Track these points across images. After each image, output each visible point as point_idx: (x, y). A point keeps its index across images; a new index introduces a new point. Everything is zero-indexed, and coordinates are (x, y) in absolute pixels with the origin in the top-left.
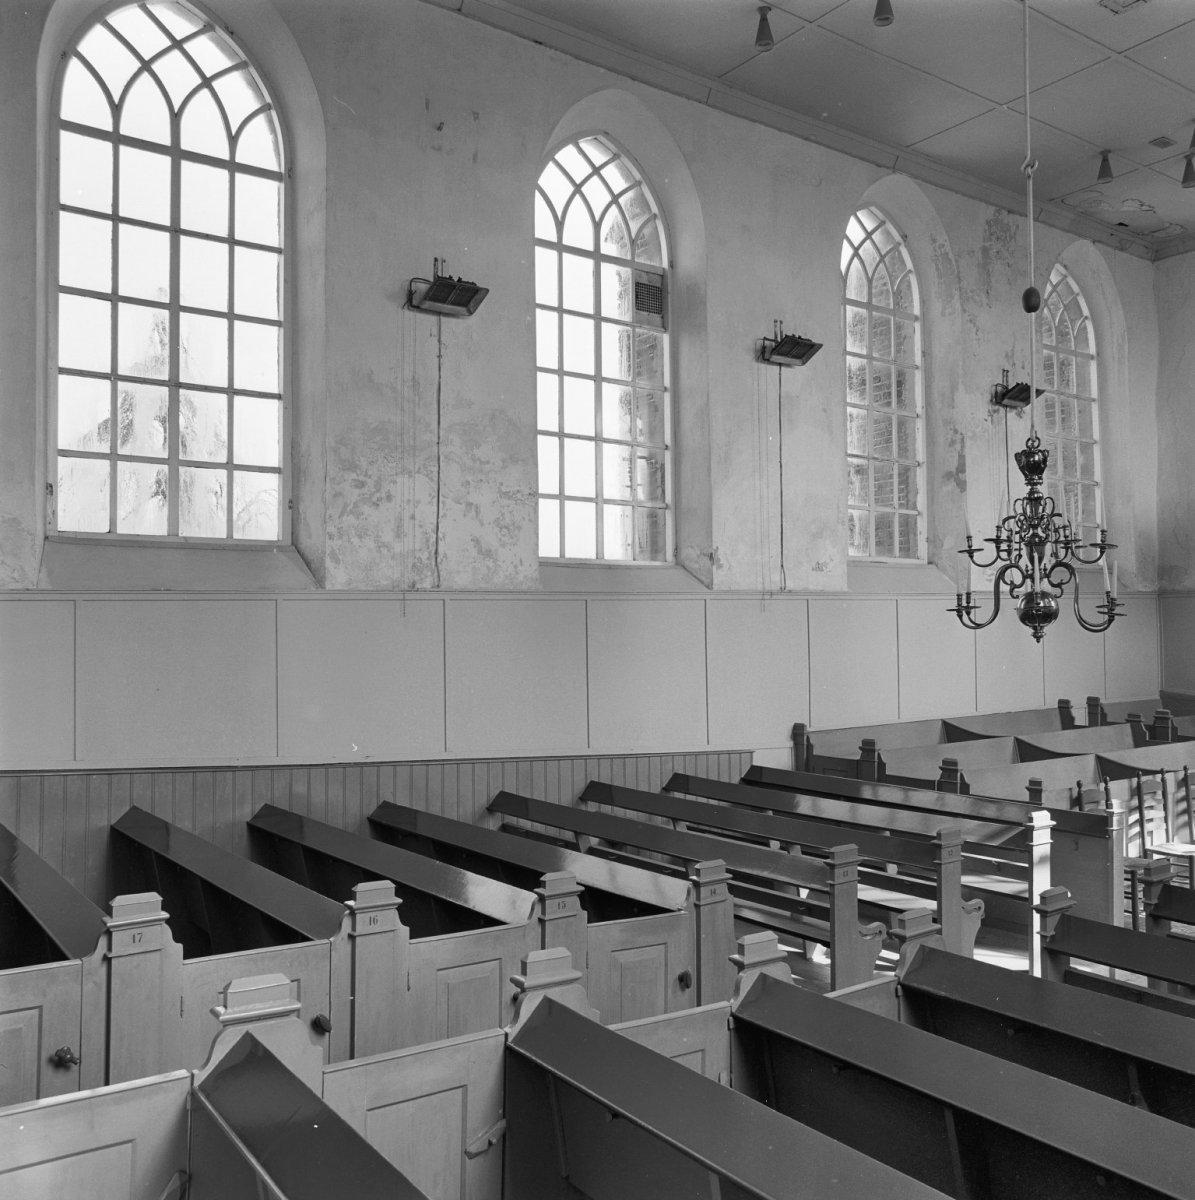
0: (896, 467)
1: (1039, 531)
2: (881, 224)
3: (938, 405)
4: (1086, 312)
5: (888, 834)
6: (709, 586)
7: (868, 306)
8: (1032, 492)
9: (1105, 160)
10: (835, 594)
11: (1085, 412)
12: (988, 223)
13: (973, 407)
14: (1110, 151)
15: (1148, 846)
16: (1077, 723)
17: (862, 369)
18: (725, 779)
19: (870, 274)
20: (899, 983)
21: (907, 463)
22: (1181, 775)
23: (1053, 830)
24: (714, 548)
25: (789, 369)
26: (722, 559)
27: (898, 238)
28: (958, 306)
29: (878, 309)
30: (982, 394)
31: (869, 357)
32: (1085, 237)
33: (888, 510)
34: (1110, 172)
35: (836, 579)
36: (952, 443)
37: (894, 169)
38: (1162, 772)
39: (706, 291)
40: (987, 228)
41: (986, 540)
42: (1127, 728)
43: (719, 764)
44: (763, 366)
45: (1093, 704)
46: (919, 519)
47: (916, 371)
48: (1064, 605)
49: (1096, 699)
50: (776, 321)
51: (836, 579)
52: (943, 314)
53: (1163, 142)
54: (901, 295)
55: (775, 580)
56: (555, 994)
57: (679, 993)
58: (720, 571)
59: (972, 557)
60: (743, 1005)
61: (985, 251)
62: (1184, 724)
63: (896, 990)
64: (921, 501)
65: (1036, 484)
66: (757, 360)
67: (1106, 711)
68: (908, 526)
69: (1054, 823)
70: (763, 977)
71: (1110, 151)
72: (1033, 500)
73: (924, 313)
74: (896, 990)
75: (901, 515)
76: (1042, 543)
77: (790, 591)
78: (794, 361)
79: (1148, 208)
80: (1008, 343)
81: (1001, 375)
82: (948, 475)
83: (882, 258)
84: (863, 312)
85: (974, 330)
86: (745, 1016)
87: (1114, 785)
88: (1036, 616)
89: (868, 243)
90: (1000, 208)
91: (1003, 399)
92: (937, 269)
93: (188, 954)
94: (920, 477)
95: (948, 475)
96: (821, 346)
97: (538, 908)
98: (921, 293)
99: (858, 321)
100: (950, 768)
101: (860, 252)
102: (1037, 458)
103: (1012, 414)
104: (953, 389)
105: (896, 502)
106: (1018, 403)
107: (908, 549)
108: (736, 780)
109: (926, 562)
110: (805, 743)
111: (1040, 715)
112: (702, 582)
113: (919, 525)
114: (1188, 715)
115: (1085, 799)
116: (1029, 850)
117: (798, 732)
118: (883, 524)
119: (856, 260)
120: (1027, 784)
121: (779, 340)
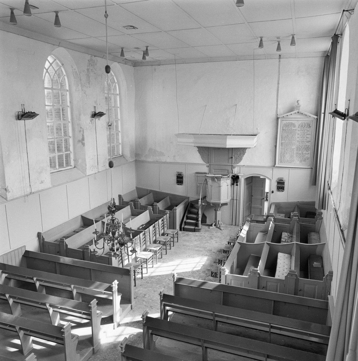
4: (116, 81)
6: (6, 199)
7: (52, 89)
13: (86, 119)
14: (123, 48)
15: (137, 256)
17: (51, 110)
19: (52, 78)
24: (7, 186)
26: (10, 189)
27: (60, 65)
28: (80, 88)
29: (55, 89)
30: (88, 115)
35: (48, 184)
36: (80, 131)
40: (88, 62)
43: (15, 255)
46: (71, 154)
47: (68, 108)
49: (121, 195)
50: (22, 105)
61: (88, 70)
64: (71, 148)
67: (123, 198)
68: (68, 156)
69: (118, 282)
71: (123, 48)
75: (65, 154)
80: (94, 99)
82: (79, 141)
83: (56, 72)
84: (50, 91)
85: (86, 96)
92: (74, 76)
94: (71, 141)
95: (79, 141)
99: (49, 93)
101: (48, 71)
103: (97, 120)
104: (80, 115)
107: (68, 164)
113: (71, 156)
114: (151, 277)
117: (39, 235)
119: (47, 73)
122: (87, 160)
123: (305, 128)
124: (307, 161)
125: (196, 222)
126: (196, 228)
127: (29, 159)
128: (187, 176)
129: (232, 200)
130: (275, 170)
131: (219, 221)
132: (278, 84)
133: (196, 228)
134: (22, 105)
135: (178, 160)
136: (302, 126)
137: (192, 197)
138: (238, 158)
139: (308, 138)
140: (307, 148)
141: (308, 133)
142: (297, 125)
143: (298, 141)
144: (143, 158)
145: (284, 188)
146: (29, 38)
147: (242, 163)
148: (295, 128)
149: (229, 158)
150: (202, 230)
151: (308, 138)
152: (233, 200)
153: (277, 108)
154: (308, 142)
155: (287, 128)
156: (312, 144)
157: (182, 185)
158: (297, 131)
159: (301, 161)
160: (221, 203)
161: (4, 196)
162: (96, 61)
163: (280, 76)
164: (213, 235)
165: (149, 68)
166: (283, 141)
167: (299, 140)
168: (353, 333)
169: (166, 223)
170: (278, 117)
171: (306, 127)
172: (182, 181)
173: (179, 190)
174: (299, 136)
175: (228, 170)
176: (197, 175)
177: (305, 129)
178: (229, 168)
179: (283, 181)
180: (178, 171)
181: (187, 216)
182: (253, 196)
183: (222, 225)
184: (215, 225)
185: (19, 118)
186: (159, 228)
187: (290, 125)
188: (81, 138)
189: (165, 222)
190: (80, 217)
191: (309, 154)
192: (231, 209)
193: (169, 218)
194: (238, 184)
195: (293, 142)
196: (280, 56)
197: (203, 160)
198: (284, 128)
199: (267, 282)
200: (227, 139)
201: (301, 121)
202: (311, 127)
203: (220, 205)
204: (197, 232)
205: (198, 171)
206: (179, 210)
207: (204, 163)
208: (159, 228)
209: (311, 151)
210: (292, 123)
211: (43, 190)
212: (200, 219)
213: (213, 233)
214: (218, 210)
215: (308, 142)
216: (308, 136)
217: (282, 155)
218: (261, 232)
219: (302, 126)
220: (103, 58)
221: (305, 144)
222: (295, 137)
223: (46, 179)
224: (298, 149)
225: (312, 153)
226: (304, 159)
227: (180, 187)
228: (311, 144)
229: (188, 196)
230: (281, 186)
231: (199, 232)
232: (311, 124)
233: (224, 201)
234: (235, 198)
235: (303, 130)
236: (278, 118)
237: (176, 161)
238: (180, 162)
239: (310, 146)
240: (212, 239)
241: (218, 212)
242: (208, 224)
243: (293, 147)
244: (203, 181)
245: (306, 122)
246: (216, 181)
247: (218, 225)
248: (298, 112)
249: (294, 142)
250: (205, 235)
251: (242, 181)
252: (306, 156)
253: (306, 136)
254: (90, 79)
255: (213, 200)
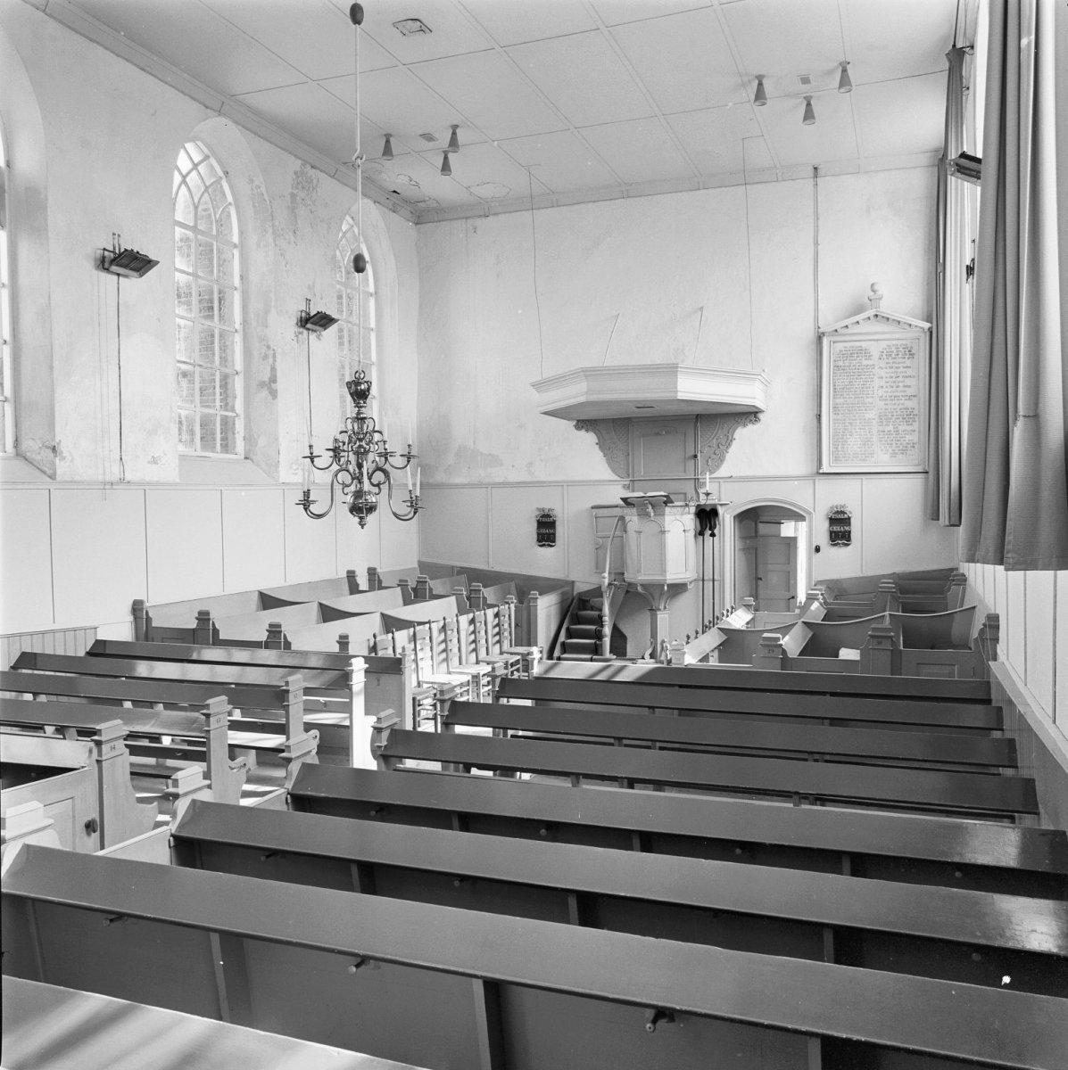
0: (218, 373)
1: (363, 443)
2: (207, 158)
3: (254, 324)
5: (233, 686)
6: (52, 477)
7: (194, 229)
8: (358, 413)
9: (388, 142)
10: (171, 484)
11: (367, 339)
12: (295, 173)
13: (283, 328)
16: (361, 588)
17: (189, 287)
18: (71, 653)
19: (196, 201)
20: (288, 793)
21: (227, 371)
22: (441, 624)
23: (367, 671)
25: (126, 280)
27: (221, 173)
28: (271, 240)
29: (202, 233)
30: (290, 317)
31: (195, 275)
32: (369, 197)
33: (211, 411)
34: (391, 152)
35: (168, 471)
36: (265, 357)
37: (220, 113)
38: (429, 622)
39: (46, 196)
41: (327, 450)
42: (398, 590)
44: (103, 275)
45: (372, 572)
48: (381, 500)
50: (114, 234)
51: (168, 471)
52: (258, 246)
53: (429, 137)
54: (222, 223)
55: (114, 472)
56: (33, 840)
57: (86, 837)
58: (62, 463)
59: (313, 462)
60: (181, 826)
61: (293, 196)
62: (437, 586)
63: (287, 798)
64: (239, 405)
65: (361, 407)
66: (97, 268)
67: (381, 577)
68: (227, 425)
69: (367, 666)
70: (304, 765)
72: (360, 419)
73: (241, 242)
74: (287, 798)
76: (367, 452)
77: (129, 482)
78: (131, 273)
79: (414, 183)
81: (304, 303)
84: (190, 234)
86: (184, 834)
87: (398, 635)
88: (361, 509)
89: (194, 173)
90: (305, 162)
91: (307, 323)
92: (254, 206)
93: (131, 754)
94: (238, 385)
95: (262, 385)
96: (157, 263)
97: (95, 751)
98: (240, 227)
100: (274, 631)
102: (363, 387)
103: (313, 336)
104: (267, 312)
105: (218, 403)
106: (317, 328)
107: (227, 446)
108: (81, 653)
109: (243, 457)
110: (145, 617)
111: (332, 583)
112: (44, 472)
113: (237, 426)
115: (379, 647)
116: (349, 687)
117: (137, 608)
118: (206, 423)
119: (183, 186)
120: (338, 639)
121: (117, 252)
122: (284, 443)
127: (129, 377)
128: (566, 518)
131: (663, 642)
132: (816, 243)
134: (114, 234)
135: (541, 474)
137: (584, 580)
139: (910, 387)
140: (909, 417)
141: (909, 372)
142: (875, 354)
144: (440, 477)
145: (849, 536)
146: (142, 69)
147: (723, 471)
151: (910, 387)
153: (817, 310)
154: (910, 397)
157: (551, 546)
158: (876, 370)
159: (894, 454)
160: (669, 582)
161: (47, 469)
162: (315, 181)
163: (820, 222)
165: (459, 225)
166: (837, 401)
168: (1024, 368)
169: (506, 626)
170: (821, 330)
171: (900, 356)
172: (554, 534)
173: (545, 563)
174: (882, 383)
175: (685, 494)
176: (595, 511)
178: (689, 488)
181: (568, 629)
185: (103, 265)
186: (486, 632)
188: (266, 377)
189: (505, 630)
190: (257, 594)
192: (698, 614)
193: (517, 625)
194: (716, 531)
196: (816, 169)
197: (614, 470)
198: (841, 363)
201: (887, 342)
202: (916, 357)
203: (666, 588)
205: (596, 504)
206: (546, 609)
207: (617, 478)
208: (486, 632)
209: (919, 422)
211: (157, 484)
212: (607, 641)
214: (660, 610)
215: (910, 397)
216: (908, 381)
220: (333, 177)
221: (903, 404)
223: (160, 455)
225: (924, 422)
227: (546, 552)
228: (919, 403)
229: (571, 578)
230: (840, 530)
232: (915, 347)
233: (674, 577)
234: (708, 575)
235: (895, 365)
236: (820, 338)
237: (535, 480)
238: (545, 480)
239: (916, 408)
243: (867, 416)
244: (608, 526)
245: (900, 342)
246: (652, 514)
247: (661, 656)
248: (877, 316)
249: (870, 400)
251: (727, 520)
252: (908, 437)
253: (903, 382)
254: (299, 221)
255: (640, 574)
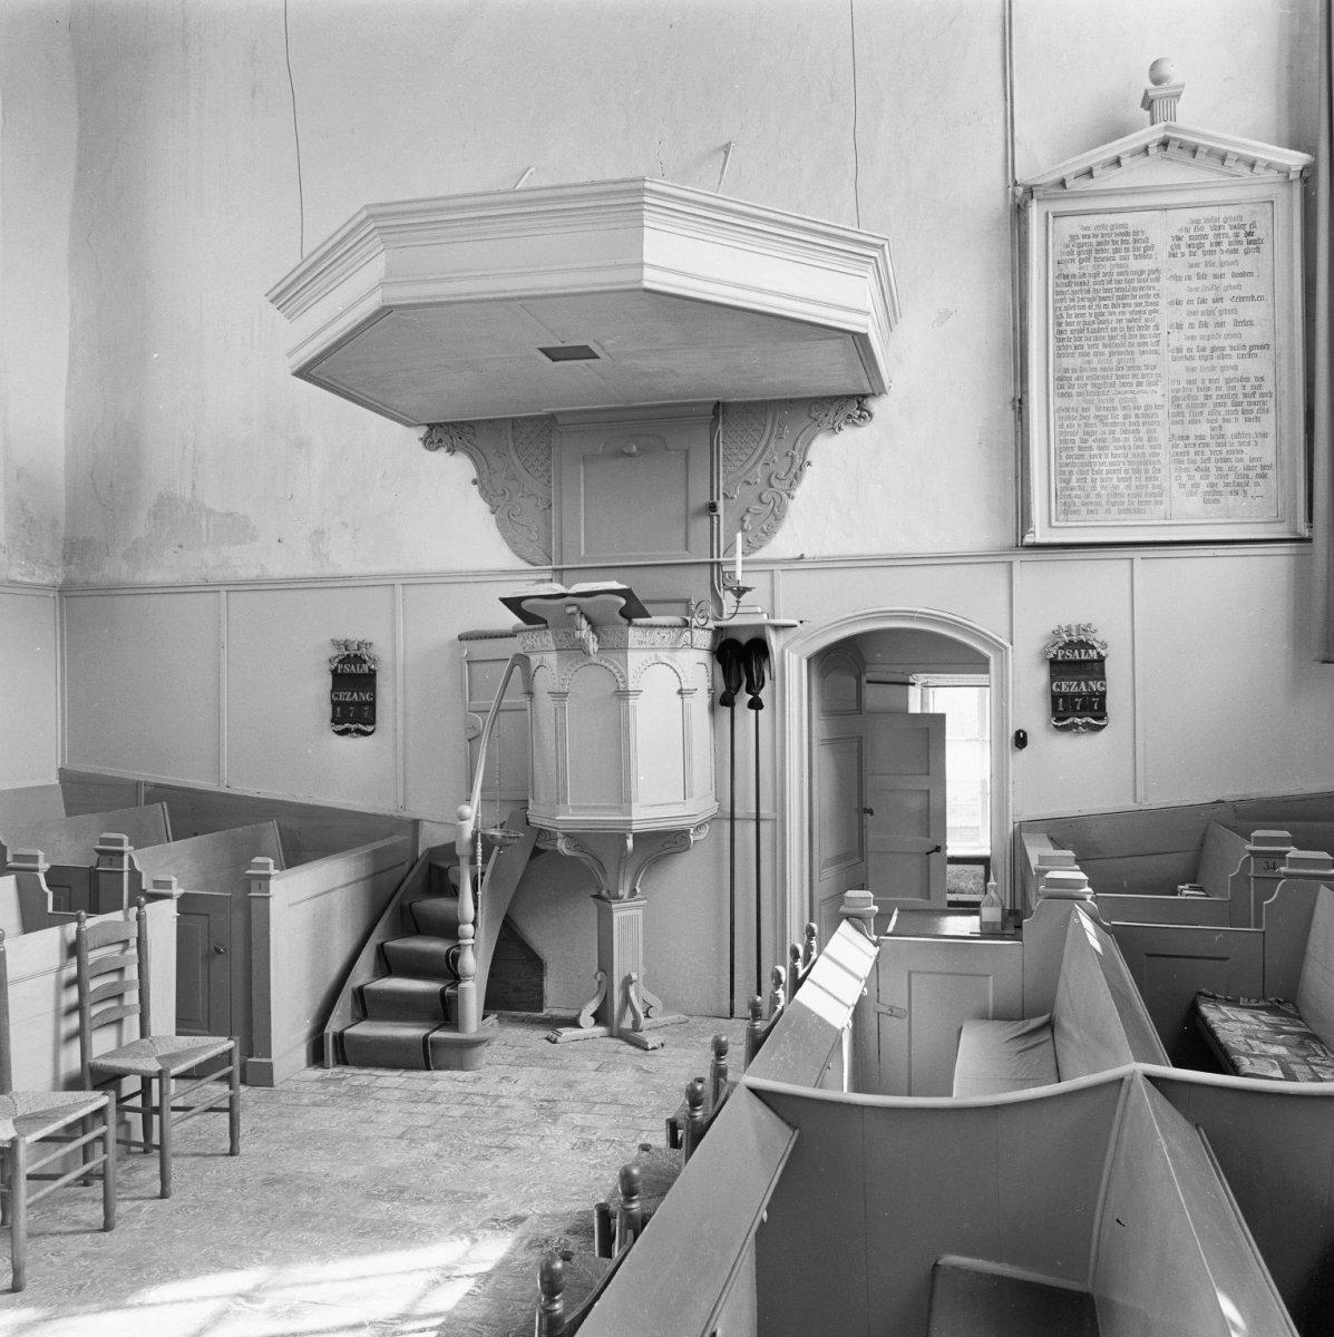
123: (1225, 257)
124: (1260, 490)
125: (443, 991)
126: (437, 1034)
129: (727, 825)
130: (1031, 575)
131: (628, 981)
133: (437, 1034)
136: (1200, 246)
138: (756, 507)
139: (1249, 323)
140: (1249, 401)
143: (1179, 350)
144: (114, 569)
145: (1102, 706)
147: (782, 544)
148: (1146, 264)
149: (688, 516)
150: (485, 1054)
152: (732, 819)
153: (1010, 141)
154: (1251, 351)
155: (1089, 267)
156: (1284, 362)
159: (1212, 496)
160: (636, 827)
164: (569, 1085)
166: (1067, 362)
167: (1186, 344)
171: (1225, 246)
173: (349, 773)
177: (1222, 265)
178: (696, 585)
179: (1093, 654)
180: (341, 637)
181: (381, 949)
182: (871, 812)
183: (658, 1018)
184: (600, 1017)
187: (1110, 247)
191: (1271, 441)
195: (1141, 360)
197: (513, 544)
198: (1073, 268)
199: (204, 915)
200: (649, 219)
202: (1265, 248)
203: (630, 843)
204: (447, 1068)
207: (523, 565)
210: (1124, 226)
213: (571, 1077)
214: (618, 898)
215: (1251, 351)
216: (1249, 311)
217: (1071, 459)
218: (983, 1016)
219: (1196, 245)
222: (1157, 327)
224: (1184, 405)
226: (1231, 479)
229: (414, 811)
230: (1077, 687)
231: (462, 1067)
234: (745, 807)
235: (1210, 271)
239: (1269, 377)
240: (555, 1117)
241: (621, 914)
242: (555, 1012)
243: (1142, 400)
246: (593, 646)
249: (1150, 359)
250: (504, 1088)
251: (790, 665)
252: (1249, 452)
253: (1234, 311)
255: (570, 810)
